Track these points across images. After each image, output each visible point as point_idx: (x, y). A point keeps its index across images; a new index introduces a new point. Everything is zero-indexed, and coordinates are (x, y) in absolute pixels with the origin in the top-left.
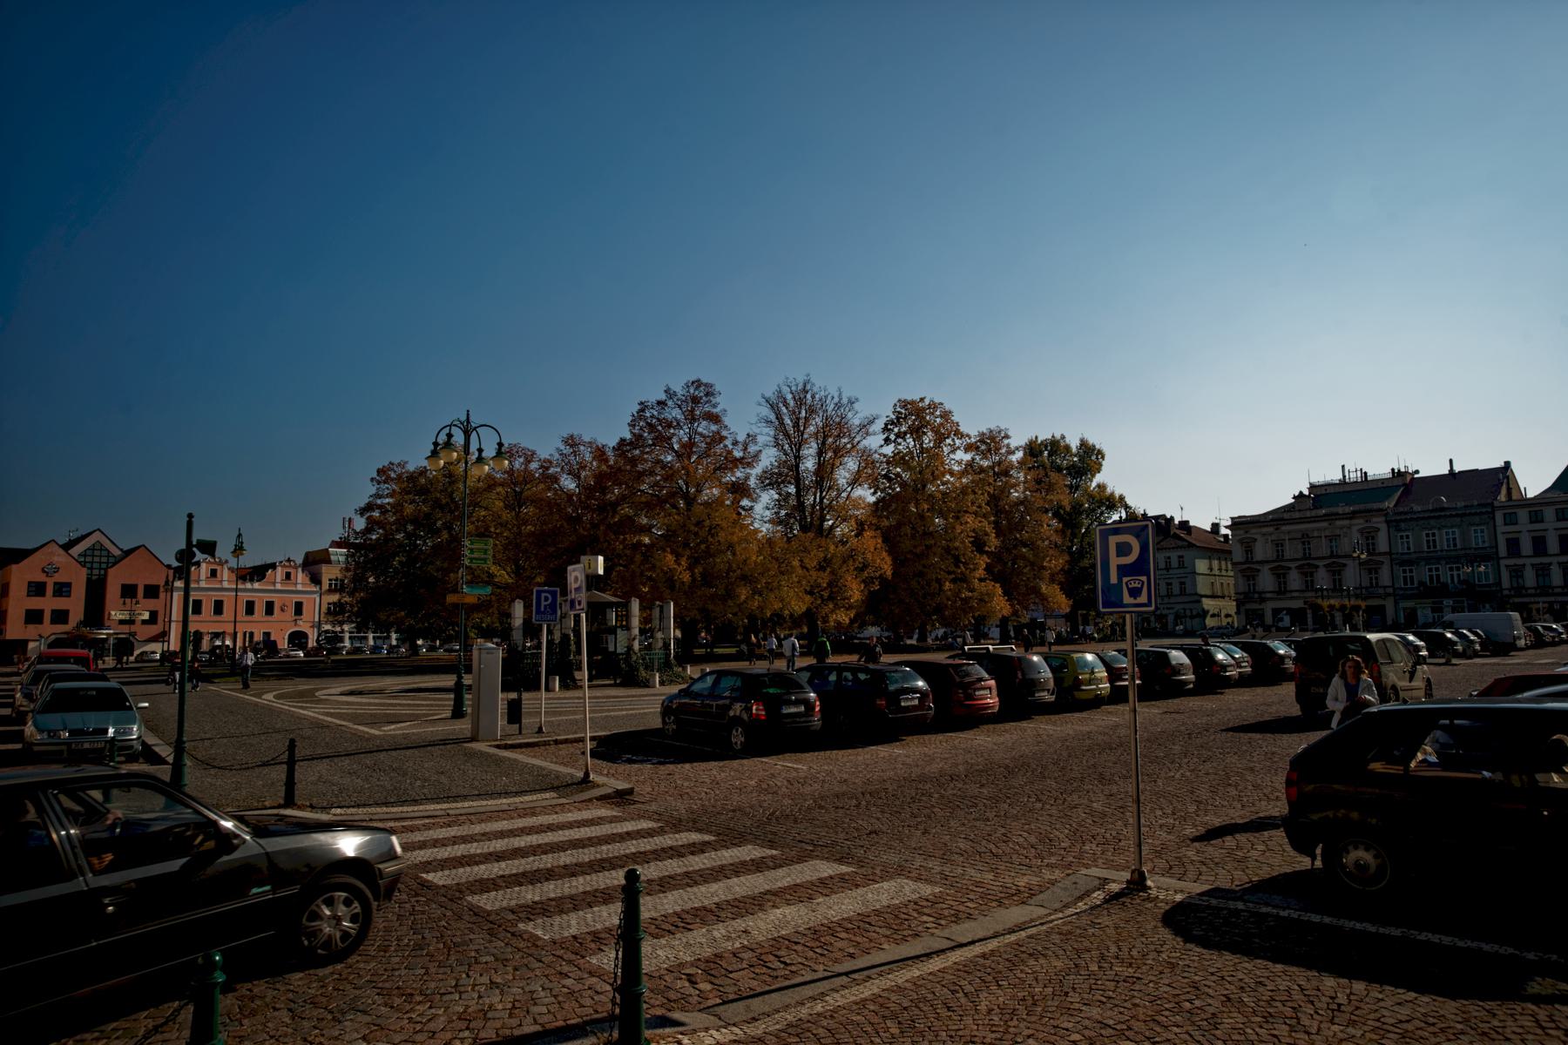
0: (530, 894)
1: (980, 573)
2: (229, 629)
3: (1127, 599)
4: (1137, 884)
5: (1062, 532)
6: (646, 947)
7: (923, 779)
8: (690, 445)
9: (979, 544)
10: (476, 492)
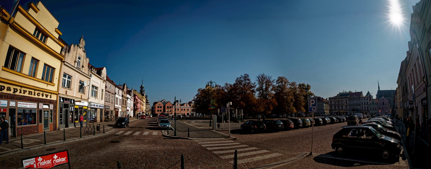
0: (221, 152)
1: (292, 105)
2: (180, 113)
3: (313, 110)
4: (311, 154)
5: (304, 99)
6: (238, 161)
7: (281, 138)
8: (245, 84)
9: (292, 101)
10: (212, 92)
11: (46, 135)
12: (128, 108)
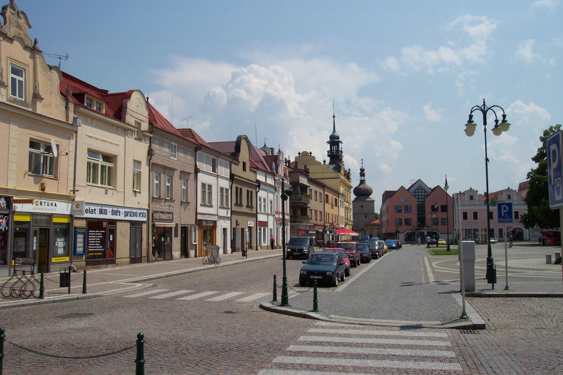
11: (45, 280)
12: (261, 218)
